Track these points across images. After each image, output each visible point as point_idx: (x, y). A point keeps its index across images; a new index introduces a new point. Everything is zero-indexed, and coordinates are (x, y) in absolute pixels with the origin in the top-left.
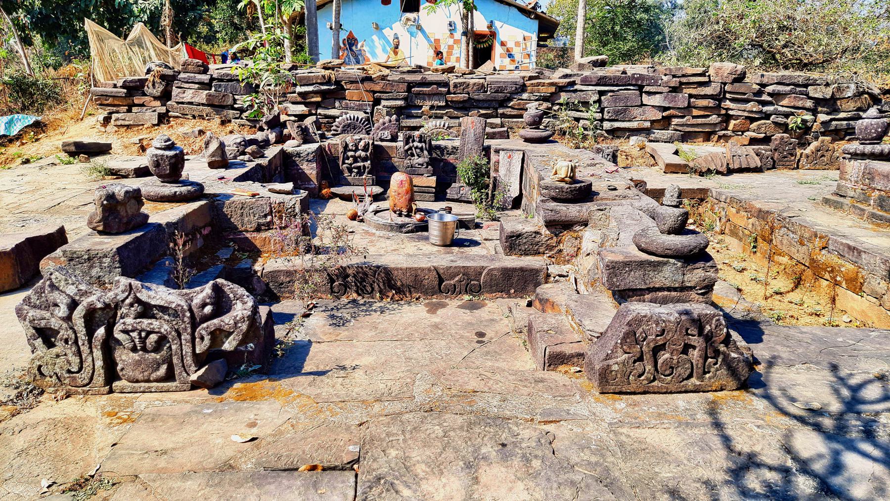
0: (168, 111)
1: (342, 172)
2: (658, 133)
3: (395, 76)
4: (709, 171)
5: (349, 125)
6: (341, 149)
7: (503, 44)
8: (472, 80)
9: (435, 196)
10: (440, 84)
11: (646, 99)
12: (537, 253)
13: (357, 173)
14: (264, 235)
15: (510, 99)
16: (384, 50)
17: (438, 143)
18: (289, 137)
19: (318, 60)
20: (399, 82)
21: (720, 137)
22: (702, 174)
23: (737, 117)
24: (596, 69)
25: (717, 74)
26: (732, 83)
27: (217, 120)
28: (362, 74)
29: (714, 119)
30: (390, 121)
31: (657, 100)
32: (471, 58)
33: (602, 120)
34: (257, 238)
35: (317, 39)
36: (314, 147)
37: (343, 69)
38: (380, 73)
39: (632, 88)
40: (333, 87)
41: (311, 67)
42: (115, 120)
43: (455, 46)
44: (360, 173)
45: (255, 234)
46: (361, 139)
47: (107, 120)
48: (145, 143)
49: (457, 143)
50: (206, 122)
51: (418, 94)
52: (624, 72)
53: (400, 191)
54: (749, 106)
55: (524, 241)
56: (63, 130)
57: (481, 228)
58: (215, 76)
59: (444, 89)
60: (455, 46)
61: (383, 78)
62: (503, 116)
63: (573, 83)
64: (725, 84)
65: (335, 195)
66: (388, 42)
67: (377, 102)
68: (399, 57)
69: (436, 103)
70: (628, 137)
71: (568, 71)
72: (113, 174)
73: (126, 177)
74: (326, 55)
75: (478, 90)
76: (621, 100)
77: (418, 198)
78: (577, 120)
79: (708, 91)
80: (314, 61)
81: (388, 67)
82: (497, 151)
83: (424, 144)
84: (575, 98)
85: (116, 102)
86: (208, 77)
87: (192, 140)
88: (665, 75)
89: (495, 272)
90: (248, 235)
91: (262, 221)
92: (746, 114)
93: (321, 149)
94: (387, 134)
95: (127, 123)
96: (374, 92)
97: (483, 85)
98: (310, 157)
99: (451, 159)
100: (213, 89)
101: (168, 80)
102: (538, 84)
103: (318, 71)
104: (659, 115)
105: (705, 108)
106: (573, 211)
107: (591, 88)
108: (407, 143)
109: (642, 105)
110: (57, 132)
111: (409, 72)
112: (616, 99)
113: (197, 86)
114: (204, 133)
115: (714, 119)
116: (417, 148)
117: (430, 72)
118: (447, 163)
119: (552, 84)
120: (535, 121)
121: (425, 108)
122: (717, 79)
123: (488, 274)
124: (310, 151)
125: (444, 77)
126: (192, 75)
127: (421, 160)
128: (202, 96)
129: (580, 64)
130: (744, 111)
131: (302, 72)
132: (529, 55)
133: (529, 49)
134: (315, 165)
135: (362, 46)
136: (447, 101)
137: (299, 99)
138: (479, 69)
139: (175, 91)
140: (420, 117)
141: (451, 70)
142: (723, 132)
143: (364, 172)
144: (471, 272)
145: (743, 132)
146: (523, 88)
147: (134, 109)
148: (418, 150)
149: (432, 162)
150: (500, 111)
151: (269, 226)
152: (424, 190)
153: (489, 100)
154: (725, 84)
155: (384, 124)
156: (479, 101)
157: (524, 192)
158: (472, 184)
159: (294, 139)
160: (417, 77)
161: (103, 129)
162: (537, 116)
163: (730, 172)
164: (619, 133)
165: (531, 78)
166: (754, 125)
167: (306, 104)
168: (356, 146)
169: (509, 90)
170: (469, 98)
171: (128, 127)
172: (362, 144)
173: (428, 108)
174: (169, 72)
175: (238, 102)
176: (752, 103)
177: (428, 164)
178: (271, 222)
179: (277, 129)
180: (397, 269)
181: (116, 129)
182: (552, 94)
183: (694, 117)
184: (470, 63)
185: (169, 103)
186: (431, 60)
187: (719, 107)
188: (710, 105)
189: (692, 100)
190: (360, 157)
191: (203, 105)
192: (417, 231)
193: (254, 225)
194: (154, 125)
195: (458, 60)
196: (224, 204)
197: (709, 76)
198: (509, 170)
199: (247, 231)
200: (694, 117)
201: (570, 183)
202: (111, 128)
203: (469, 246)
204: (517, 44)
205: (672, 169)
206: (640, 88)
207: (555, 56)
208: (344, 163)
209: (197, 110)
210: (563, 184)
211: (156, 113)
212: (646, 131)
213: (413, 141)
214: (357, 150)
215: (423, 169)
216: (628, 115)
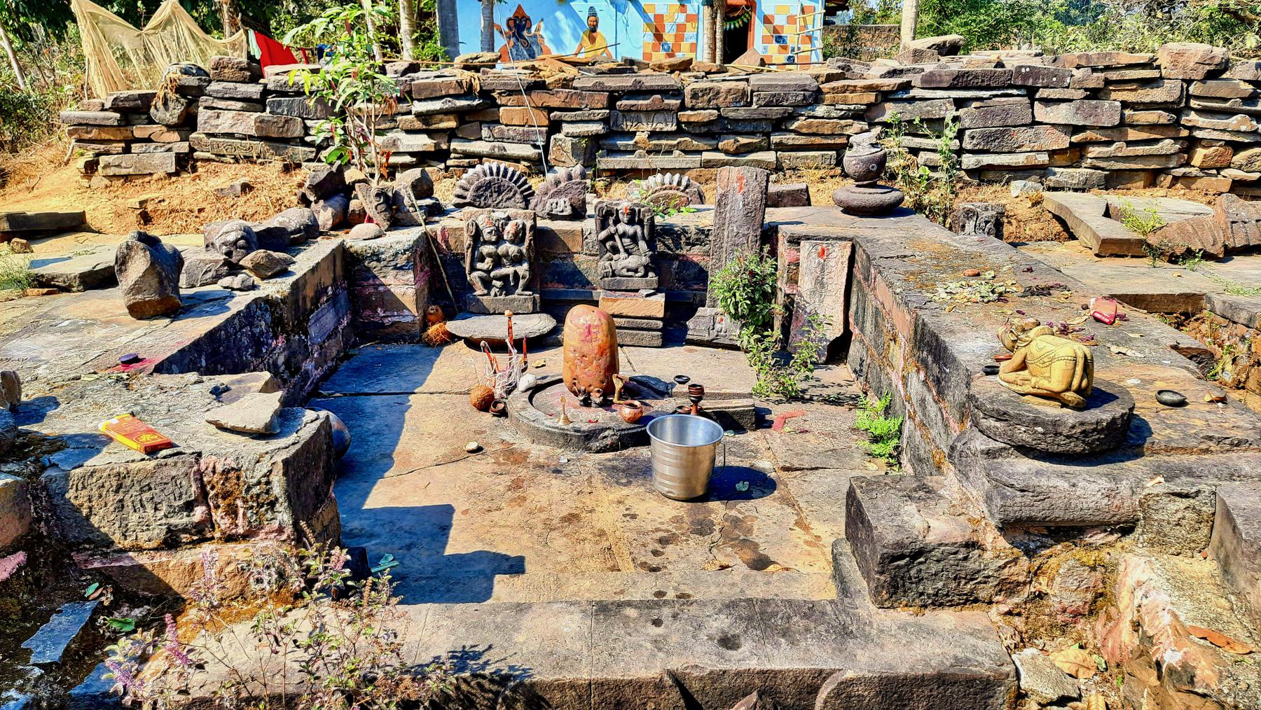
0: (192, 150)
1: (471, 288)
2: (1062, 174)
3: (586, 80)
4: (1189, 254)
5: (488, 185)
6: (467, 241)
7: (767, 20)
8: (723, 84)
9: (663, 337)
10: (665, 92)
11: (1041, 112)
12: (971, 600)
13: (501, 289)
14: (187, 556)
15: (792, 117)
16: (576, 37)
17: (669, 220)
18: (361, 217)
19: (458, 54)
20: (593, 90)
21: (1176, 179)
22: (1173, 259)
23: (1209, 143)
24: (944, 59)
25: (1175, 64)
26: (1203, 81)
27: (278, 164)
28: (528, 78)
29: (1167, 146)
30: (570, 177)
31: (1061, 114)
32: (719, 44)
33: (960, 152)
34: (170, 568)
35: (455, 16)
36: (407, 237)
37: (499, 66)
38: (562, 75)
39: (1015, 92)
40: (476, 102)
41: (446, 66)
42: (104, 168)
43: (689, 25)
44: (508, 288)
45: (163, 557)
46: (508, 219)
47: (91, 167)
48: (150, 207)
49: (707, 220)
50: (257, 167)
51: (628, 111)
52: (1000, 64)
53: (585, 350)
54: (1234, 122)
55: (934, 568)
56: (33, 182)
57: (769, 425)
58: (270, 87)
59: (675, 102)
60: (689, 25)
61: (566, 83)
62: (781, 147)
63: (907, 86)
64: (1189, 82)
65: (453, 338)
66: (579, 20)
67: (555, 127)
68: (597, 45)
69: (660, 127)
70: (1008, 183)
71: (894, 64)
72: (42, 285)
73: (67, 289)
74: (470, 46)
75: (736, 101)
76: (995, 115)
77: (628, 341)
78: (915, 151)
79: (1157, 95)
80: (450, 56)
81: (574, 64)
82: (795, 241)
83: (638, 228)
84: (913, 112)
85: (105, 136)
86: (259, 88)
87: (230, 202)
88: (1078, 67)
89: (860, 690)
90: (143, 560)
91: (180, 520)
92: (1227, 137)
93: (427, 239)
94: (563, 205)
95: (124, 172)
96: (550, 110)
97: (744, 93)
98: (401, 260)
99: (695, 254)
100: (268, 109)
101: (190, 95)
102: (845, 89)
103: (456, 74)
104: (1063, 141)
105: (1152, 127)
106: (1086, 489)
107: (939, 94)
108: (604, 225)
109: (1035, 123)
110: (22, 186)
111: (612, 72)
112: (987, 113)
113: (239, 105)
114: (251, 188)
115: (1167, 146)
117: (649, 71)
118: (686, 264)
119: (870, 88)
120: (869, 171)
121: (641, 137)
122: (1173, 73)
123: (837, 693)
124: (400, 247)
125: (673, 80)
126: (231, 85)
127: (633, 261)
128: (249, 123)
129: (915, 51)
130: (1224, 131)
131: (422, 77)
132: (810, 38)
133: (810, 28)
134: (411, 276)
135: (538, 30)
136: (679, 123)
137: (418, 125)
138: (735, 63)
139: (203, 115)
140: (632, 152)
141: (685, 66)
142: (1183, 170)
143: (516, 286)
144: (785, 686)
145: (1219, 170)
146: (817, 97)
147: (135, 147)
148: (627, 241)
149: (657, 263)
150: (775, 138)
151: (201, 533)
152: (638, 325)
153: (755, 120)
154: (1189, 82)
155: (557, 183)
156: (736, 121)
157: (855, 330)
158: (743, 316)
159: (370, 220)
160: (626, 82)
161: (85, 183)
162: (870, 161)
163: (1230, 253)
164: (991, 175)
165: (830, 78)
166: (1241, 157)
167: (431, 133)
168: (499, 233)
169: (791, 100)
170: (720, 116)
171: (127, 178)
172: (510, 229)
173: (645, 135)
174: (192, 81)
175: (312, 132)
176: (1239, 117)
177: (647, 268)
178: (209, 522)
179: (338, 200)
180: (561, 687)
181: (107, 182)
182: (869, 106)
183: (1129, 143)
184: (719, 53)
185: (193, 135)
186: (649, 50)
187: (1177, 124)
188: (1162, 121)
189: (1128, 112)
190: (506, 255)
191: (251, 137)
192: (625, 447)
193: (158, 533)
194: (170, 175)
195: (694, 47)
196: (67, 477)
197: (1158, 67)
198: (820, 283)
199: (140, 550)
200: (1129, 143)
201: (1079, 408)
202: (98, 180)
203: (747, 496)
204: (791, 20)
205: (1112, 249)
206: (1031, 92)
207: (836, 40)
208: (473, 269)
209: (242, 147)
210: (1051, 410)
211: (172, 154)
212: (1040, 171)
213: (617, 221)
214: (499, 241)
215: (636, 281)
216: (1008, 144)
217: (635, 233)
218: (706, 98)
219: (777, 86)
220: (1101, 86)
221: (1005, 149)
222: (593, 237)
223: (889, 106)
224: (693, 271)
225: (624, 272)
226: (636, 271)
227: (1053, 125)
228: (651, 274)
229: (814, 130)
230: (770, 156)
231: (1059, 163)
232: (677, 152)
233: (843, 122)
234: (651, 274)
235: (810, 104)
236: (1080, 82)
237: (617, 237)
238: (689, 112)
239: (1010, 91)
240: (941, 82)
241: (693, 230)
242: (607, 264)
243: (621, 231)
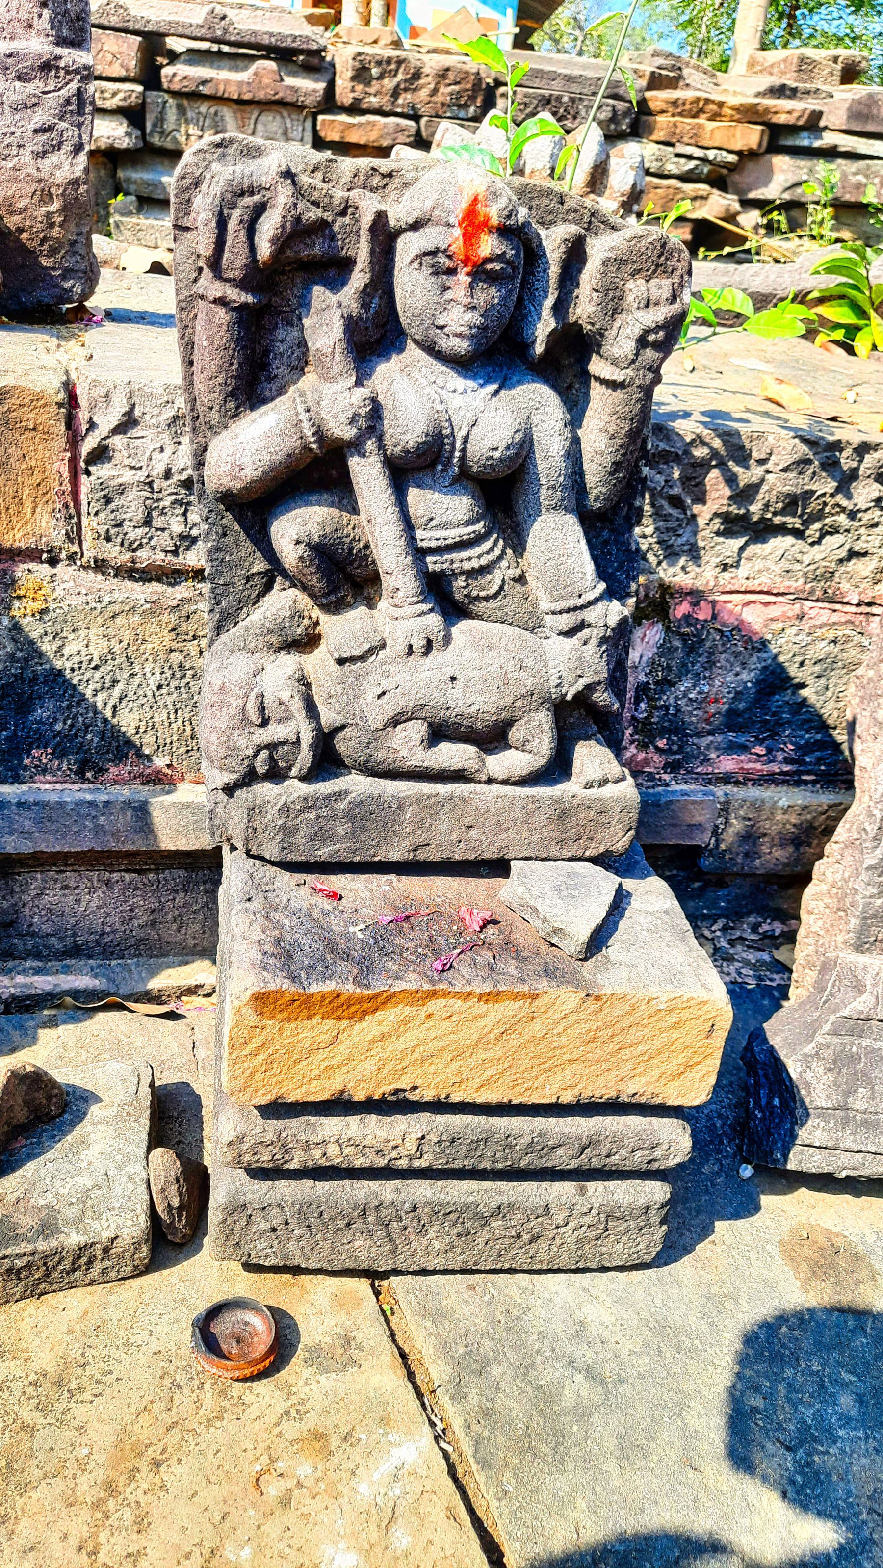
59: (309, 87)
116: (421, 464)
127: (481, 664)
148: (445, 511)
182: (747, 156)
213: (375, 336)
217: (522, 454)
218: (389, 83)
219: (553, 76)
222: (157, 452)
223: (781, 162)
224: (730, 680)
225: (408, 745)
226: (493, 737)
228: (591, 758)
233: (688, 187)
234: (591, 758)
237: (367, 473)
238: (343, 118)
241: (777, 448)
242: (279, 674)
243: (406, 429)
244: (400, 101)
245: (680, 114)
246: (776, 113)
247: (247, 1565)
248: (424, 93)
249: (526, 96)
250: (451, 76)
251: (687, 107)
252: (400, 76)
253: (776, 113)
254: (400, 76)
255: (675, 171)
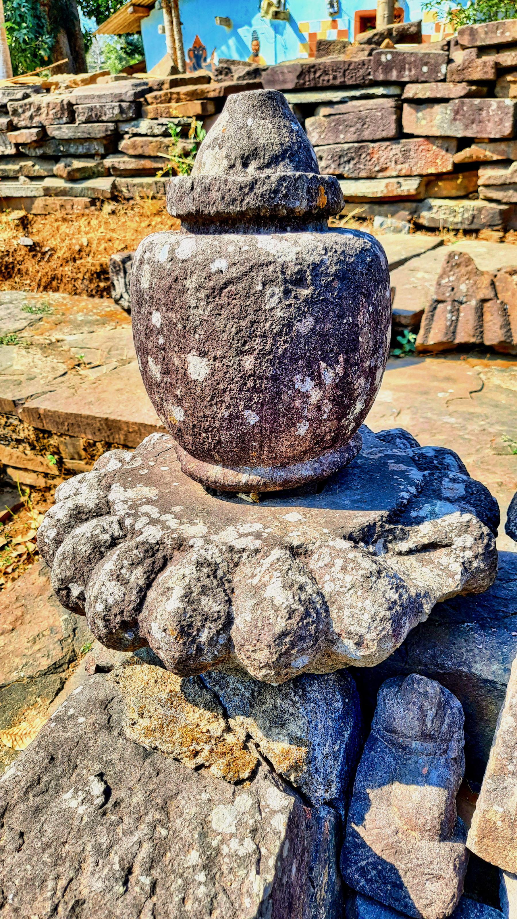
11: (414, 121)
31: (436, 121)
39: (380, 91)
104: (445, 162)
112: (337, 123)
150: (108, 162)
218: (28, 114)
220: (490, 75)
221: (363, 174)
227: (427, 137)
229: (139, 151)
230: (103, 184)
231: (445, 193)
232: (22, 178)
235: (132, 119)
236: (461, 71)
239: (371, 91)
240: (284, 82)
244: (34, 121)
245: (161, 102)
246: (208, 92)
247: (515, 101)
248: (44, 116)
249: (82, 108)
250: (51, 106)
251: (163, 98)
252: (32, 110)
253: (208, 92)
254: (32, 110)
255: (159, 133)
